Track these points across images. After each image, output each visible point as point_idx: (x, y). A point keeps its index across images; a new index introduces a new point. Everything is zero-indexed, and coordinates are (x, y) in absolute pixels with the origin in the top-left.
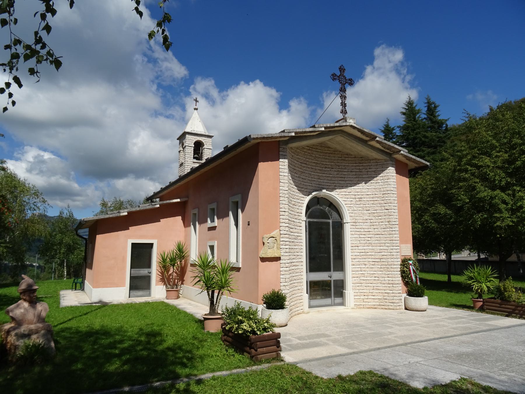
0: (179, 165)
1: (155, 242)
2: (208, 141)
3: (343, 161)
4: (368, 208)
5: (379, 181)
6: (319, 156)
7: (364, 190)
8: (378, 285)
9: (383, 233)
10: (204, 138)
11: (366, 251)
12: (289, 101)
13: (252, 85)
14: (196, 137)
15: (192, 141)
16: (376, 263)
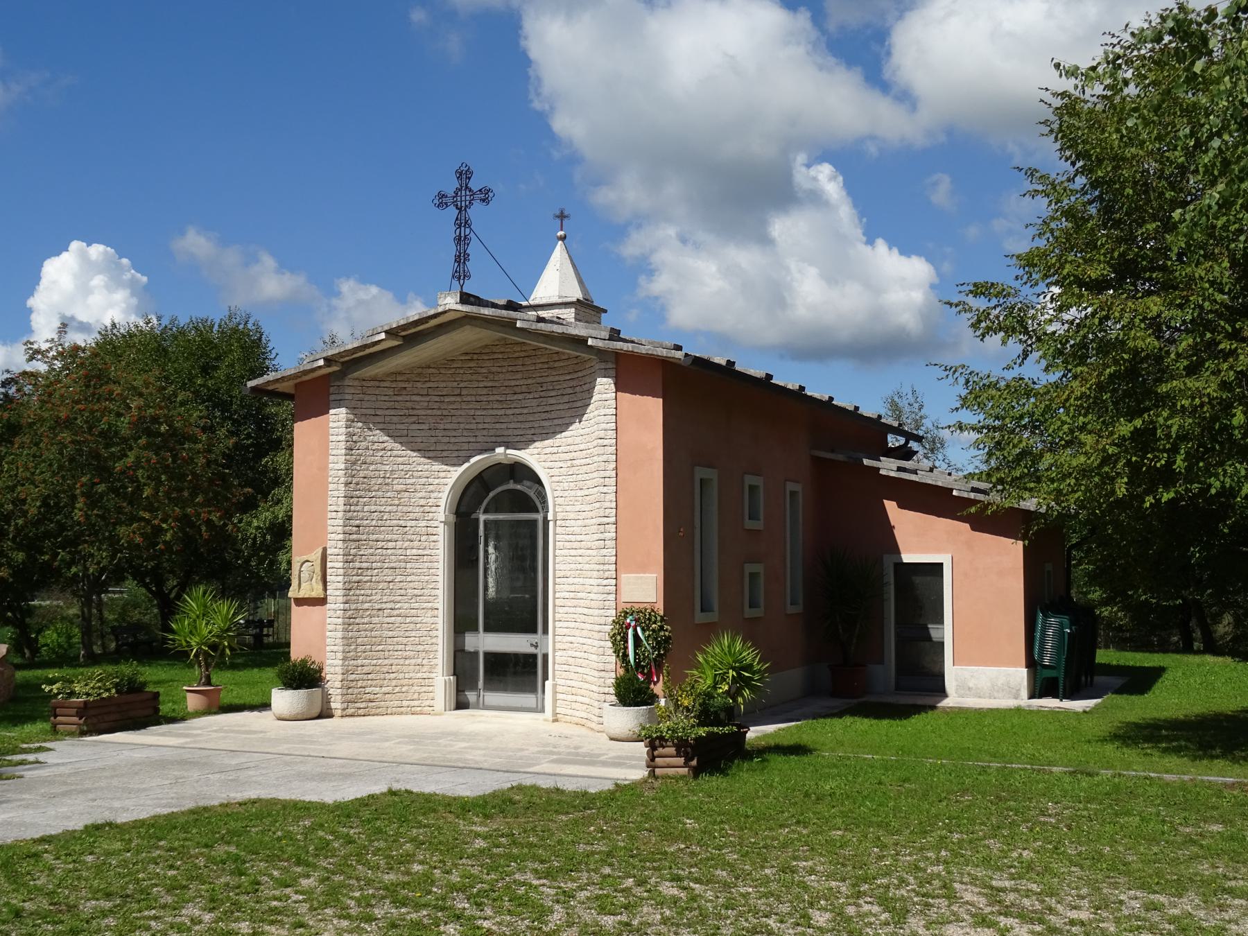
3: (550, 371)
6: (499, 370)
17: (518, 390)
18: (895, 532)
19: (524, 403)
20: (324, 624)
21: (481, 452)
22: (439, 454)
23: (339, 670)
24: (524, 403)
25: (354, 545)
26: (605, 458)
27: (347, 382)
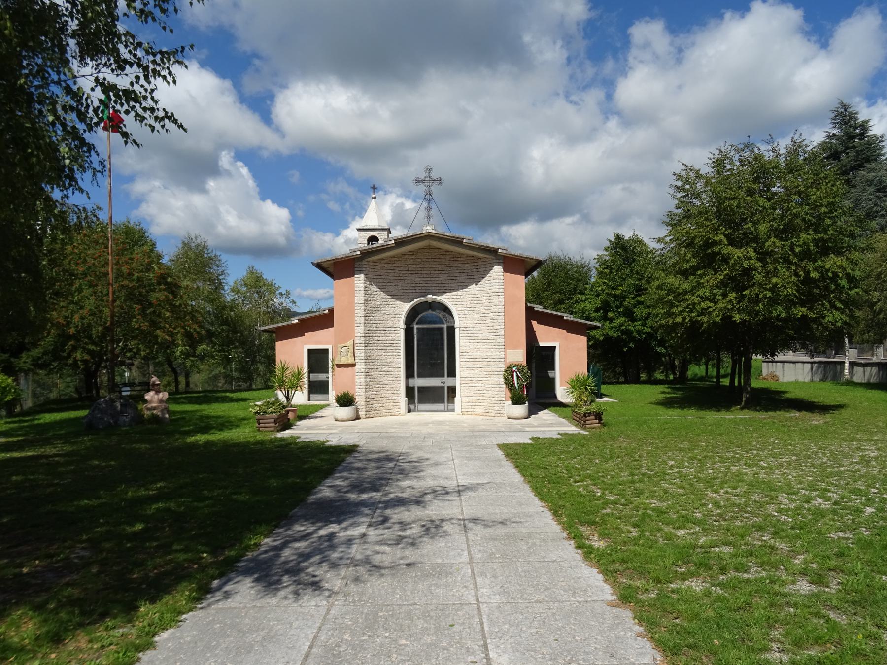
1: (329, 347)
4: (478, 312)
5: (487, 282)
7: (474, 293)
8: (485, 392)
9: (489, 338)
11: (475, 357)
16: (483, 370)
17: (437, 269)
18: (565, 331)
19: (440, 275)
20: (354, 376)
21: (421, 296)
22: (399, 297)
23: (363, 397)
24: (440, 275)
25: (367, 338)
26: (499, 300)
27: (364, 262)
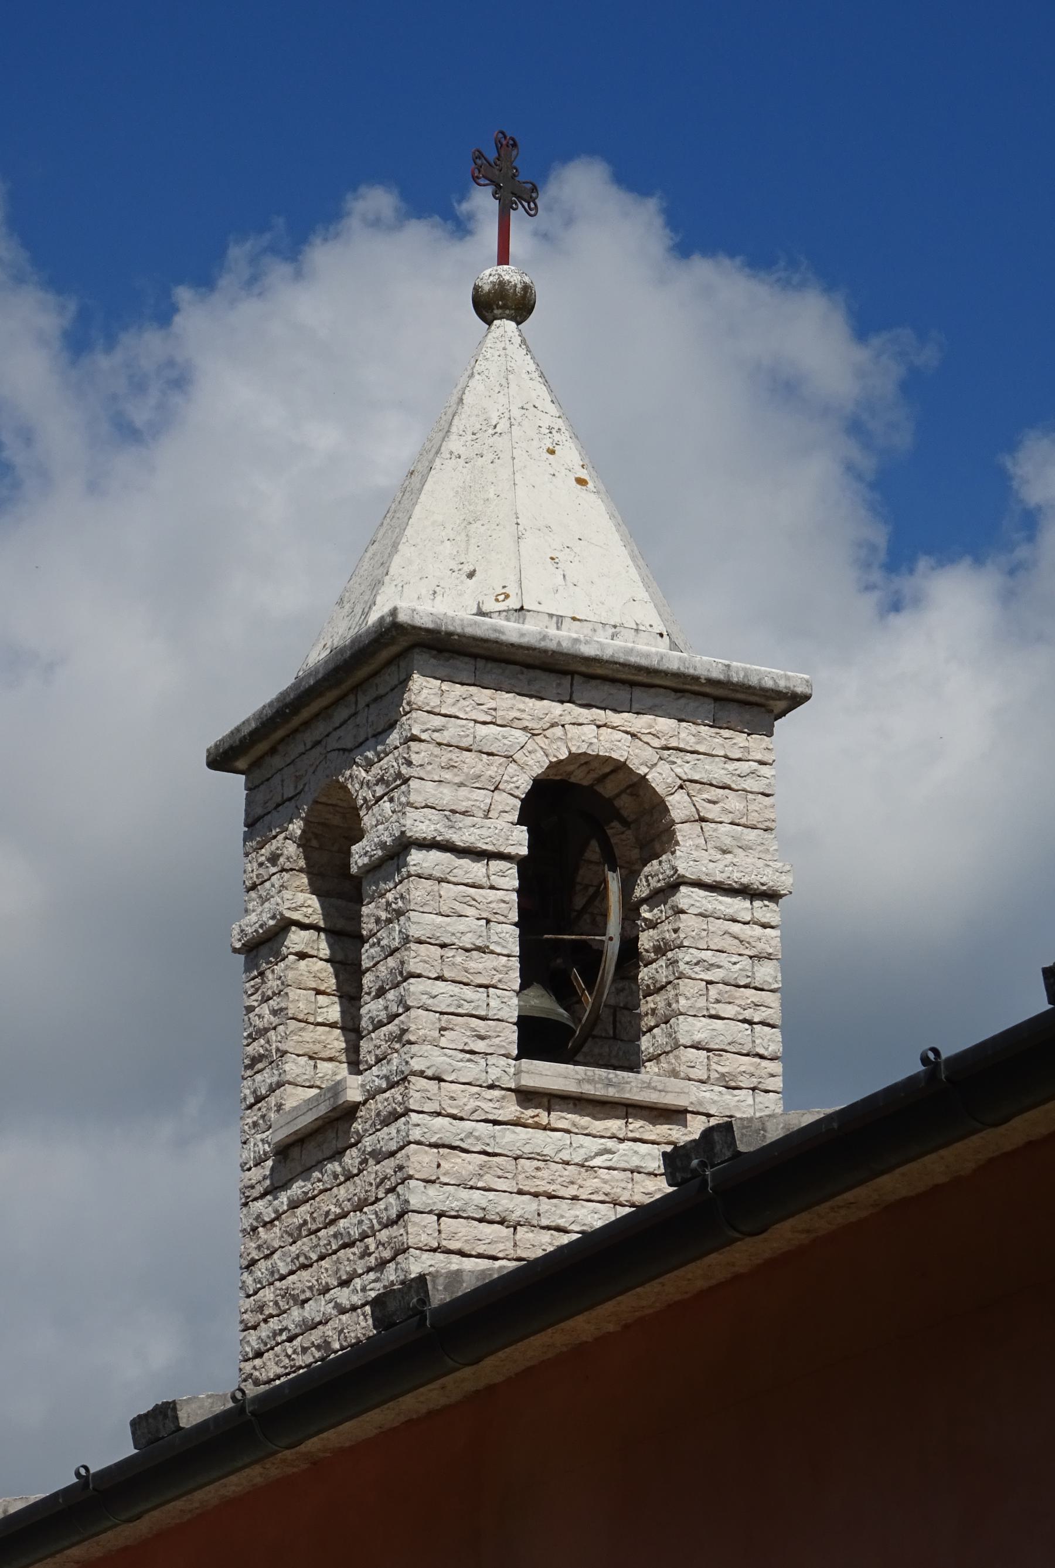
0: (261, 1143)
2: (717, 771)
10: (664, 724)
12: (1012, 446)
13: (668, 231)
14: (556, 709)
15: (493, 768)
